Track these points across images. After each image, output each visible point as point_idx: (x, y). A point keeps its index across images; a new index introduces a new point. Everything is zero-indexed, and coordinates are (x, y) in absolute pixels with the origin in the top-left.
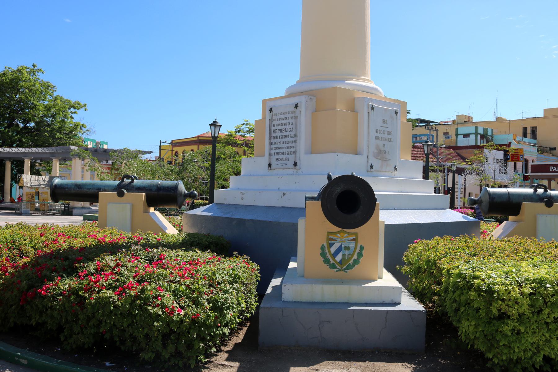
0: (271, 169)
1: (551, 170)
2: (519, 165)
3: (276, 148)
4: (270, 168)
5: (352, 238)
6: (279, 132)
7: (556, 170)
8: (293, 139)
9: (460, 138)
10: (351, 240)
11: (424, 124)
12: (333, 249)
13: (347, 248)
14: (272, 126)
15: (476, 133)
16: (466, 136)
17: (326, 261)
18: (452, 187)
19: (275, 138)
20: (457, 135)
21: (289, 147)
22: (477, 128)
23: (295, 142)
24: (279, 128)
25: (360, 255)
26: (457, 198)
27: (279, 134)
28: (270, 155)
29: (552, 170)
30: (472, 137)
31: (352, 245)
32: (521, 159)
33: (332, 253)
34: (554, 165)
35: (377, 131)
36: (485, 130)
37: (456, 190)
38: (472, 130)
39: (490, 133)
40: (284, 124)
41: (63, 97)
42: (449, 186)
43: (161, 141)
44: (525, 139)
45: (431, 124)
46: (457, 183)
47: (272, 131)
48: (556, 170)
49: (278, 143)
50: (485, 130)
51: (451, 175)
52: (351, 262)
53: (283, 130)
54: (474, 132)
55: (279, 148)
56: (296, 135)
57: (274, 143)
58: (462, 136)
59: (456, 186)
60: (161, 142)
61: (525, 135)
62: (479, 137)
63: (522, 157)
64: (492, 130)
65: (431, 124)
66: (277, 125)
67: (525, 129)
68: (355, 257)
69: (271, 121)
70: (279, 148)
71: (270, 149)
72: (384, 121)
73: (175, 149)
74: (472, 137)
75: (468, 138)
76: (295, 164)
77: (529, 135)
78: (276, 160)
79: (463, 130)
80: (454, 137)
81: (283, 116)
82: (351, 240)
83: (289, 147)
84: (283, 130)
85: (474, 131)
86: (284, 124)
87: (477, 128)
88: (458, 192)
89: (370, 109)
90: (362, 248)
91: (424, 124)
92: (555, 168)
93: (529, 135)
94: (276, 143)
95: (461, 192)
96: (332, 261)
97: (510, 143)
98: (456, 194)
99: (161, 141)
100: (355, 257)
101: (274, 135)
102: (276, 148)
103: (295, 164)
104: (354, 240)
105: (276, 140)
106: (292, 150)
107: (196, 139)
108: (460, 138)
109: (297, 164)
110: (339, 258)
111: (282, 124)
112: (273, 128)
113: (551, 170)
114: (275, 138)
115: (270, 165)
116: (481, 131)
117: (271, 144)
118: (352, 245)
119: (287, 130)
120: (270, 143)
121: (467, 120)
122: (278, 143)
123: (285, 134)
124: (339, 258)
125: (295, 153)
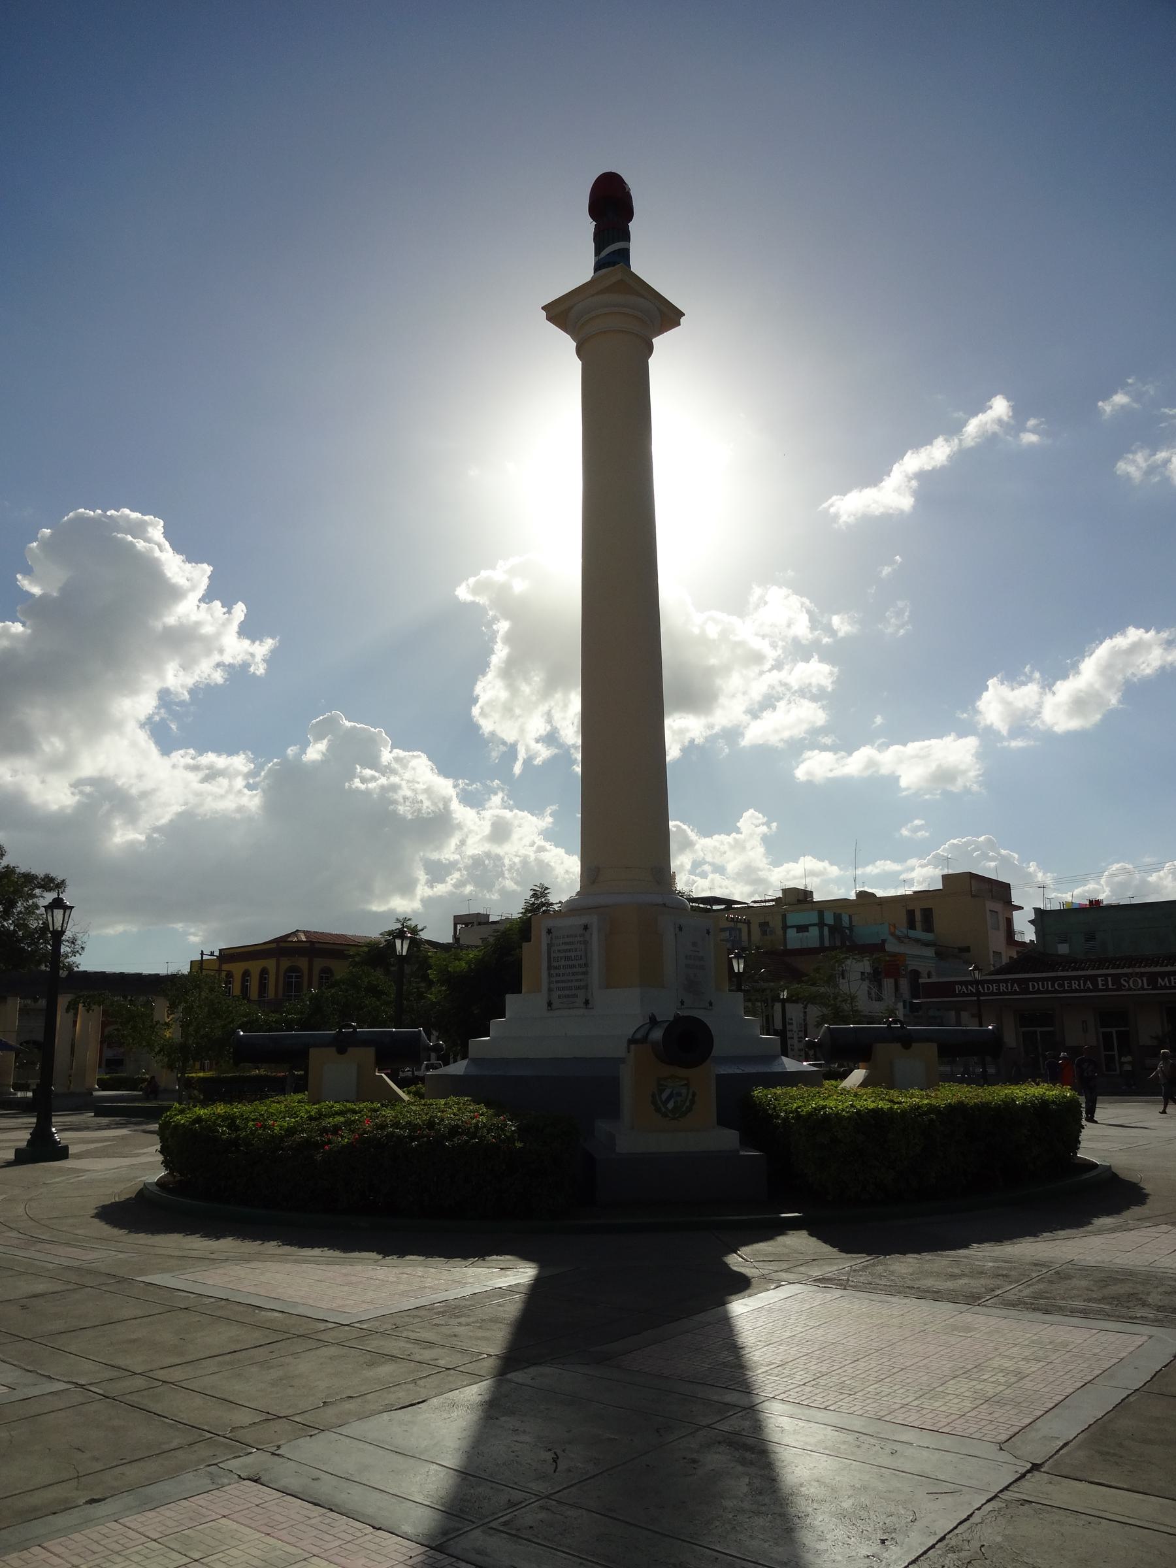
0: (551, 1010)
1: (957, 992)
2: (904, 983)
3: (557, 982)
4: (549, 1008)
5: (683, 1083)
6: (563, 960)
7: (966, 992)
8: (584, 970)
9: (792, 933)
10: (683, 1086)
11: (723, 907)
12: (665, 1096)
13: (679, 1094)
14: (552, 952)
15: (821, 924)
16: (802, 929)
17: (658, 1110)
18: (781, 1028)
19: (556, 968)
20: (785, 927)
21: (577, 980)
22: (821, 914)
23: (585, 973)
24: (562, 955)
25: (693, 1102)
26: (792, 1050)
27: (563, 963)
28: (550, 990)
29: (959, 991)
30: (814, 931)
31: (684, 1091)
32: (904, 973)
33: (664, 1099)
34: (961, 983)
35: (686, 957)
36: (838, 917)
37: (789, 1034)
38: (813, 918)
39: (846, 921)
40: (569, 950)
41: (53, 875)
42: (776, 1027)
43: (202, 951)
44: (912, 933)
45: (736, 906)
46: (791, 1021)
47: (552, 960)
48: (966, 992)
49: (561, 975)
50: (838, 917)
51: (778, 1007)
52: (684, 1109)
53: (569, 958)
54: (816, 921)
55: (563, 982)
56: (586, 965)
57: (555, 975)
58: (795, 930)
59: (789, 1027)
60: (202, 954)
61: (912, 925)
62: (826, 930)
63: (903, 970)
64: (850, 917)
65: (736, 906)
66: (559, 951)
67: (911, 914)
68: (688, 1104)
69: (549, 946)
70: (563, 982)
71: (549, 983)
72: (694, 944)
73: (225, 967)
74: (814, 931)
75: (806, 934)
76: (587, 1002)
77: (918, 925)
78: (559, 997)
79: (795, 919)
80: (780, 932)
81: (567, 940)
82: (683, 1086)
83: (577, 980)
84: (569, 958)
85: (816, 921)
86: (569, 950)
87: (821, 914)
88: (793, 1038)
89: (677, 930)
90: (694, 1095)
91: (723, 907)
92: (964, 987)
93: (918, 925)
94: (557, 975)
95: (799, 1038)
96: (663, 1110)
97: (884, 941)
98: (789, 1041)
99: (202, 951)
100: (688, 1104)
101: (555, 964)
102: (557, 982)
103: (587, 1002)
104: (686, 1085)
105: (557, 971)
106: (582, 984)
107: (274, 945)
108: (792, 933)
109: (590, 1002)
110: (670, 1105)
111: (566, 951)
112: (553, 955)
113: (957, 992)
114: (556, 968)
115: (550, 1004)
116: (829, 919)
117: (550, 975)
118: (684, 1091)
119: (573, 957)
120: (549, 974)
121: (801, 898)
122: (561, 975)
123: (570, 963)
124: (670, 1105)
125: (586, 987)
